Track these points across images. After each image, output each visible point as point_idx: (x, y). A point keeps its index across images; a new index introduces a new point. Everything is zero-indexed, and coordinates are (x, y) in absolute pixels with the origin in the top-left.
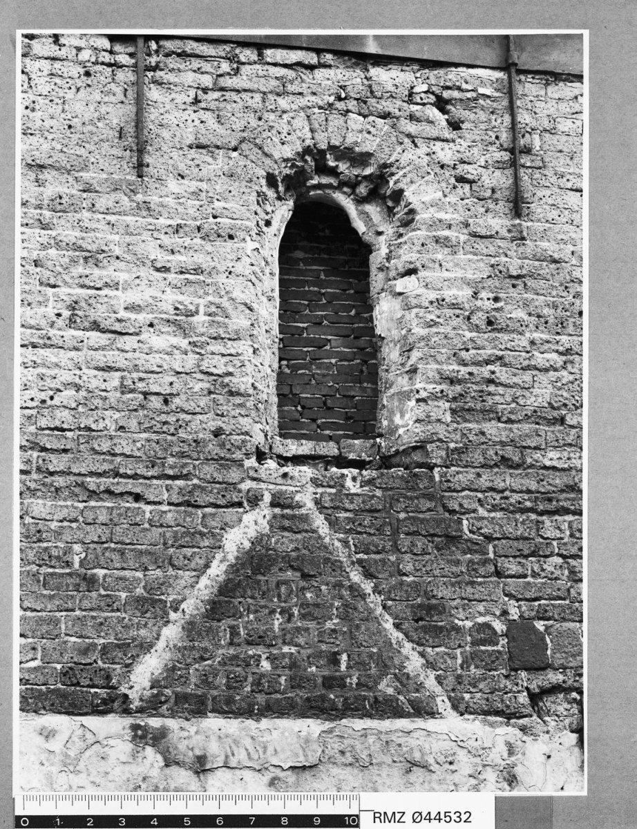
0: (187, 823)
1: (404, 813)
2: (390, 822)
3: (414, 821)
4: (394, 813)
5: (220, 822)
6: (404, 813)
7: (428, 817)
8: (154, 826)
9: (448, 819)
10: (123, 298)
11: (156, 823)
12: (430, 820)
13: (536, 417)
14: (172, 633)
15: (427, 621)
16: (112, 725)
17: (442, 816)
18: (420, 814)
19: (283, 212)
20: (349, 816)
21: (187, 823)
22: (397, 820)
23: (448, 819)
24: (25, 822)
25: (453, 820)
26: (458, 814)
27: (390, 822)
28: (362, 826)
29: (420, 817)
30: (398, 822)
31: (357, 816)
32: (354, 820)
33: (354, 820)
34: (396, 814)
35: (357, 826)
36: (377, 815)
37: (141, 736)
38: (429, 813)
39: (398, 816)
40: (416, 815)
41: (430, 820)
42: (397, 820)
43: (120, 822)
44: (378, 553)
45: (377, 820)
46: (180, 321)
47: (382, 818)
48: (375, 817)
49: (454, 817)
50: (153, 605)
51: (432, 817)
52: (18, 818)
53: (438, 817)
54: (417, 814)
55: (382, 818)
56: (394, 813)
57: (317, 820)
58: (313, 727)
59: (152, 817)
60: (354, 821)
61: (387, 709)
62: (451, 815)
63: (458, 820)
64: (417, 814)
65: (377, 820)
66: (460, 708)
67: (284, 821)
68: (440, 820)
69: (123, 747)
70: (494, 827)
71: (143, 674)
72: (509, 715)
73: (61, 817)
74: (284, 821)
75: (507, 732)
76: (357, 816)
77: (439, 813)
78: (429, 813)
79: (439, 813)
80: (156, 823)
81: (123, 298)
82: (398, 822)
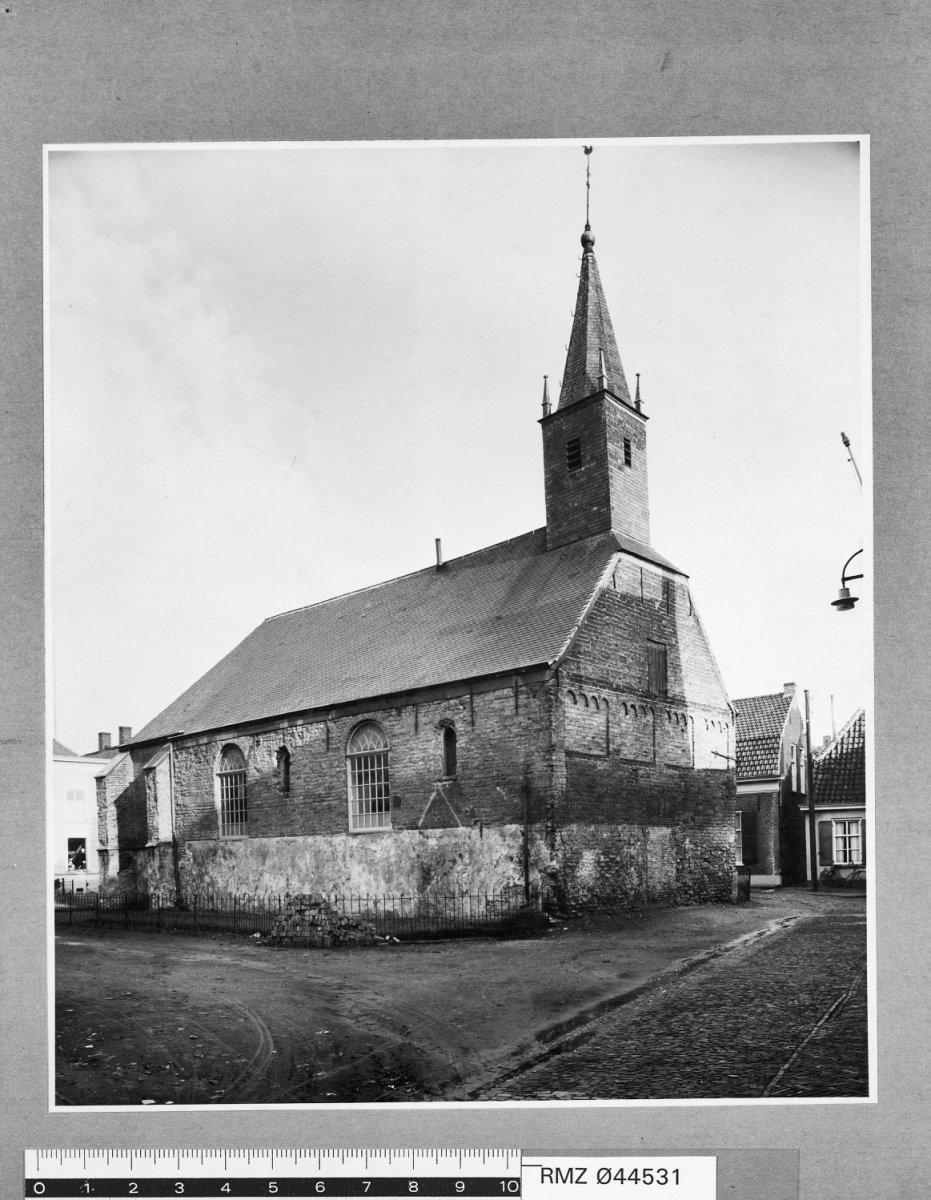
0: (273, 1189)
1: (585, 1170)
2: (564, 1182)
3: (600, 1181)
4: (571, 1170)
5: (320, 1189)
6: (585, 1170)
7: (619, 1176)
8: (225, 1194)
9: (648, 1179)
10: (416, 756)
11: (228, 1190)
12: (622, 1180)
13: (475, 768)
14: (423, 816)
15: (458, 811)
16: (416, 832)
17: (640, 1175)
18: (609, 1171)
19: (442, 732)
20: (507, 1180)
21: (273, 1189)
22: (574, 1180)
23: (648, 1179)
24: (39, 1188)
25: (655, 1182)
26: (663, 1173)
27: (564, 1182)
28: (523, 1198)
29: (608, 1176)
30: (577, 1182)
31: (518, 1180)
32: (512, 1186)
33: (512, 1186)
34: (574, 1170)
35: (518, 1194)
36: (547, 1172)
37: (421, 833)
38: (622, 1170)
39: (576, 1174)
40: (603, 1172)
41: (622, 1180)
42: (574, 1180)
43: (177, 1188)
44: (590, 617)
45: (547, 1179)
46: (423, 760)
47: (554, 1176)
48: (543, 1175)
49: (657, 1176)
50: (421, 811)
51: (626, 1176)
52: (30, 1183)
53: (633, 1177)
54: (604, 1172)
55: (554, 1176)
56: (571, 1170)
57: (460, 1185)
58: (441, 830)
59: (224, 1181)
60: (513, 1186)
61: (453, 826)
62: (653, 1173)
63: (663, 1180)
64: (604, 1172)
65: (547, 1179)
66: (463, 825)
67: (413, 1187)
68: (636, 1180)
69: (418, 835)
70: (713, 1196)
71: (420, 824)
72: (471, 826)
73: (91, 1181)
74: (413, 1187)
75: (469, 829)
76: (518, 1180)
77: (636, 1170)
78: (622, 1170)
79: (636, 1170)
80: (228, 1190)
81: (416, 756)
82: (577, 1182)
